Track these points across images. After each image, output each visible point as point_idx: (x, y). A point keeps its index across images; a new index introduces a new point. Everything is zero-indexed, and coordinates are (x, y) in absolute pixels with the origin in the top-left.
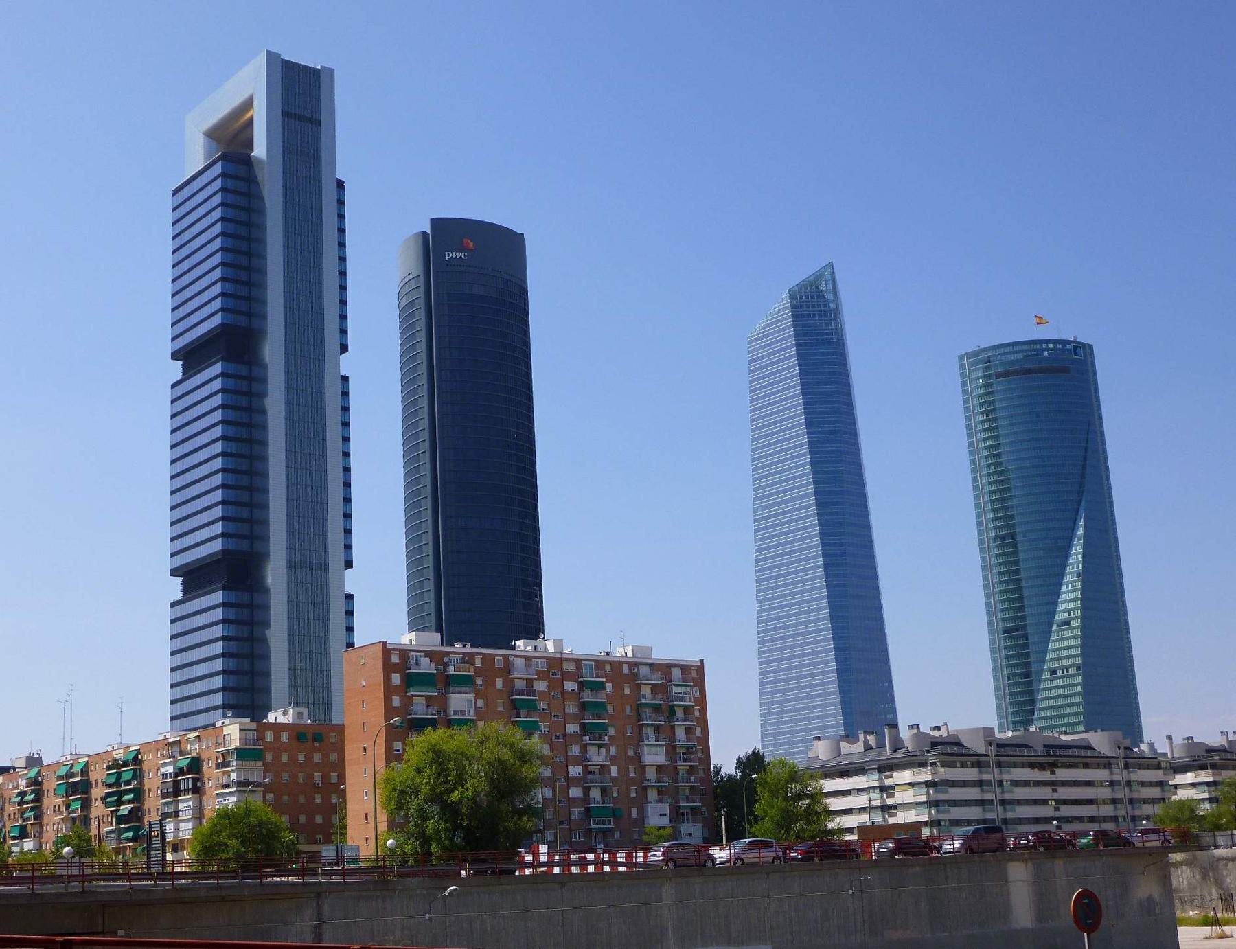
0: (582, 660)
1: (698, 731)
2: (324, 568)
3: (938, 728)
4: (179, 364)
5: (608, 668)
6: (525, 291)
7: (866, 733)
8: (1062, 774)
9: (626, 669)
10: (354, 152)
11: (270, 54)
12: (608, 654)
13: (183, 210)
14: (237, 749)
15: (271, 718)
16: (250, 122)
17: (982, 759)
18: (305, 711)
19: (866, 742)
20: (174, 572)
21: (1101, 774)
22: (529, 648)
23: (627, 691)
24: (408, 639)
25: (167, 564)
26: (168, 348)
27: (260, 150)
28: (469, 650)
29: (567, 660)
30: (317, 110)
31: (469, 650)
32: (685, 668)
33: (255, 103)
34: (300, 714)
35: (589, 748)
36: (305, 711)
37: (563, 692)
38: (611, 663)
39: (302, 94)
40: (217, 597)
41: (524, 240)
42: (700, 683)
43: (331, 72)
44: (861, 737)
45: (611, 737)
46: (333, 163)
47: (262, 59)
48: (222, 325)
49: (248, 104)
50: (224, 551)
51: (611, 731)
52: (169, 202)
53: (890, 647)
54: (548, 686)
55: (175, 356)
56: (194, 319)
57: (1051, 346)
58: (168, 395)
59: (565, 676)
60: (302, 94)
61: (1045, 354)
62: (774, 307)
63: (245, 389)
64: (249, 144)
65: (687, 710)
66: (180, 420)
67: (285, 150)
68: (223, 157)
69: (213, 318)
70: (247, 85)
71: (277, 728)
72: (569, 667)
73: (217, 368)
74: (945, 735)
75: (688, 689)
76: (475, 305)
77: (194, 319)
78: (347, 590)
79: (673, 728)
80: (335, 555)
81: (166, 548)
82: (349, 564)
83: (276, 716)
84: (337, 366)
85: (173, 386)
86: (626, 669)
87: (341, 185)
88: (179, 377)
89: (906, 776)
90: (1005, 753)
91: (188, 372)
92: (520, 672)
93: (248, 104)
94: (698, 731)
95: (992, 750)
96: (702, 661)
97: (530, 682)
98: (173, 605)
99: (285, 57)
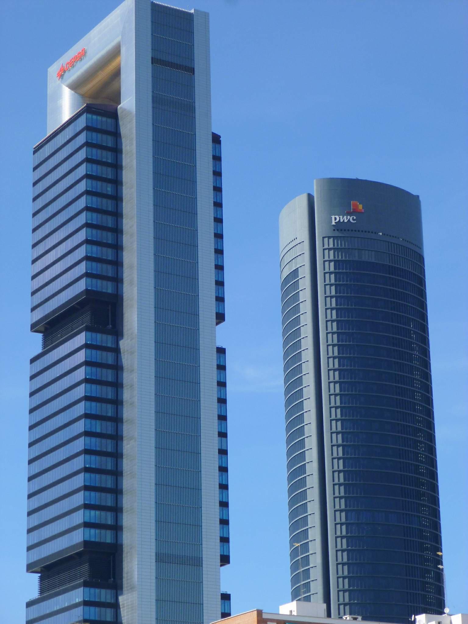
2: (197, 562)
4: (39, 337)
6: (421, 259)
10: (226, 103)
13: (41, 233)
16: (117, 74)
20: (30, 568)
25: (22, 559)
27: (128, 103)
30: (191, 58)
33: (123, 50)
40: (77, 595)
43: (206, 15)
46: (208, 114)
48: (87, 291)
49: (116, 52)
50: (86, 543)
58: (27, 370)
63: (110, 361)
64: (117, 97)
66: (37, 536)
68: (89, 109)
73: (80, 339)
78: (219, 344)
80: (210, 550)
81: (23, 540)
82: (225, 560)
85: (33, 361)
87: (216, 139)
88: (39, 350)
91: (49, 345)
93: (116, 52)
98: (29, 604)
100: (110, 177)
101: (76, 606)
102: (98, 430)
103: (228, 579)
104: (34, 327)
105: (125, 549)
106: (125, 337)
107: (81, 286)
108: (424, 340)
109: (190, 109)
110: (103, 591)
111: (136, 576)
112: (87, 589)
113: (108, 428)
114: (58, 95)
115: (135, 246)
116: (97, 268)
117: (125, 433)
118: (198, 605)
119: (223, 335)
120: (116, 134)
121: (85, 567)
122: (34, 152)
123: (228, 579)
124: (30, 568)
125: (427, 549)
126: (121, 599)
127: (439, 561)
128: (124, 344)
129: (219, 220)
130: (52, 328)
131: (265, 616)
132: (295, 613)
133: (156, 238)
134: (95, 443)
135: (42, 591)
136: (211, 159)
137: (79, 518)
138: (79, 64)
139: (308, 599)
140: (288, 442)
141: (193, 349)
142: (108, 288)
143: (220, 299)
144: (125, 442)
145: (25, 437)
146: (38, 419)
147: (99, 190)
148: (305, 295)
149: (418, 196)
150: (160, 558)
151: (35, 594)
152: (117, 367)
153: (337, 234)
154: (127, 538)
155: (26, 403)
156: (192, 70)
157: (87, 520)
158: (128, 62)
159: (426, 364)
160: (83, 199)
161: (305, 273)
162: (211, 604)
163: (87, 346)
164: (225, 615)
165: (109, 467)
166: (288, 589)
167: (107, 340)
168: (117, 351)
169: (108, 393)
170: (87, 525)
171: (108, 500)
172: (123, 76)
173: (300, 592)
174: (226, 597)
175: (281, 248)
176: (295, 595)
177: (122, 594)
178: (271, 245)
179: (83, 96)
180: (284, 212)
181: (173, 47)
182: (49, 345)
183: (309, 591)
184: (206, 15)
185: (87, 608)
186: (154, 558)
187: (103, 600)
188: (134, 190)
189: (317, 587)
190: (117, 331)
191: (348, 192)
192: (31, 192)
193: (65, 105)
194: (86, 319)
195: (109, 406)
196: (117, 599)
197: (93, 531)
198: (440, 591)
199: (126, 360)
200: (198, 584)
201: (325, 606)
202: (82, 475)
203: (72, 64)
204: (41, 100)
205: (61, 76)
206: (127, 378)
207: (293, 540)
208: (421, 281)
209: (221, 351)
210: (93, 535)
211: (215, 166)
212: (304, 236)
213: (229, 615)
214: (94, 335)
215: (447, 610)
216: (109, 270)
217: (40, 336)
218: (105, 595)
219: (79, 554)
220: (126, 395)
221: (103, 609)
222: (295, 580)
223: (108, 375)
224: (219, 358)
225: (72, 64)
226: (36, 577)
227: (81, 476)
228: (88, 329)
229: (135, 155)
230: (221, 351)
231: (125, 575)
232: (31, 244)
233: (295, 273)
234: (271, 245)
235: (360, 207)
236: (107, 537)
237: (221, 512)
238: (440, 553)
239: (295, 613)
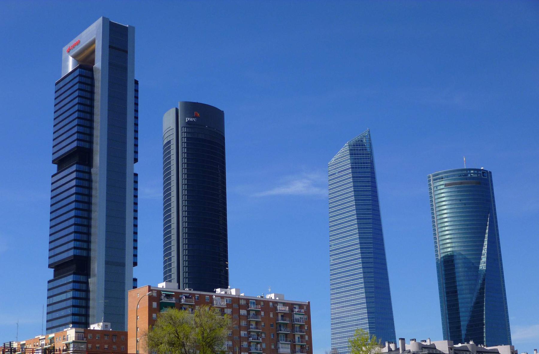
0: (249, 299)
1: (307, 337)
2: (123, 265)
3: (425, 341)
4: (56, 166)
5: (262, 304)
6: (224, 138)
7: (389, 343)
9: (271, 304)
10: (144, 68)
14: (73, 342)
15: (92, 327)
16: (93, 52)
18: (109, 324)
19: (389, 347)
22: (223, 293)
23: (271, 316)
24: (162, 285)
25: (47, 262)
26: (51, 158)
27: (98, 64)
28: (192, 292)
29: (242, 299)
31: (192, 292)
32: (301, 306)
33: (96, 42)
34: (106, 326)
35: (252, 344)
36: (109, 324)
37: (239, 315)
38: (264, 301)
40: (70, 278)
41: (223, 114)
42: (308, 312)
43: (134, 28)
44: (387, 344)
45: (263, 339)
46: (133, 72)
48: (77, 147)
50: (75, 256)
51: (263, 335)
52: (54, 89)
53: (395, 322)
54: (232, 312)
55: (54, 162)
56: (64, 144)
57: (472, 172)
59: (240, 307)
61: (469, 175)
64: (93, 62)
65: (301, 327)
67: (110, 64)
68: (80, 67)
69: (73, 144)
70: (93, 33)
71: (94, 331)
72: (243, 302)
73: (74, 168)
74: (429, 344)
75: (302, 316)
76: (204, 149)
77: (64, 144)
78: (135, 172)
79: (294, 335)
81: (47, 254)
82: (135, 264)
83: (96, 327)
84: (133, 169)
85: (53, 176)
86: (271, 304)
87: (136, 82)
88: (56, 172)
91: (60, 170)
92: (219, 303)
93: (93, 42)
94: (307, 337)
96: (309, 303)
98: (49, 282)
100: (89, 83)
101: (69, 299)
102: (81, 207)
103: (136, 272)
105: (92, 259)
106: (94, 167)
107: (75, 144)
108: (224, 178)
109: (125, 69)
110: (82, 276)
111: (98, 161)
112: (75, 276)
113: (86, 206)
114: (67, 60)
115: (99, 128)
116: (80, 213)
117: (93, 209)
118: (123, 284)
120: (92, 78)
121: (74, 266)
122: (56, 85)
123: (136, 272)
124: (50, 266)
125: (222, 261)
126: (89, 280)
127: (227, 266)
128: (93, 170)
129: (135, 233)
130: (62, 162)
131: (151, 288)
132: (164, 287)
133: (108, 185)
134: (79, 221)
135: (55, 276)
136: (134, 98)
137: (72, 245)
138: (76, 47)
139: (170, 281)
140: (164, 215)
141: (124, 175)
142: (87, 146)
143: (135, 256)
144: (93, 213)
146: (53, 239)
147: (80, 231)
148: (173, 152)
150: (107, 263)
151: (51, 277)
152: (90, 180)
153: (188, 126)
154: (93, 254)
156: (127, 52)
157: (75, 246)
158: (98, 47)
159: (225, 188)
161: (174, 142)
162: (129, 282)
163: (76, 171)
164: (135, 287)
165: (85, 247)
166: (162, 277)
167: (86, 168)
168: (90, 173)
169: (87, 109)
170: (75, 248)
171: (85, 237)
172: (96, 53)
173: (167, 278)
174: (135, 280)
175: (164, 130)
176: (165, 279)
177: (90, 278)
178: (160, 128)
179: (78, 61)
180: (166, 115)
181: (118, 39)
182: (60, 170)
183: (171, 255)
184: (134, 28)
185: (74, 284)
186: (104, 262)
187: (82, 280)
188: (99, 103)
189: (174, 276)
190: (87, 274)
191: (192, 108)
192: (52, 143)
193: (70, 65)
195: (86, 190)
196: (90, 170)
197: (76, 309)
198: (226, 279)
199: (94, 178)
200: (123, 274)
201: (177, 284)
202: (73, 227)
203: (73, 47)
204: (60, 62)
205: (68, 52)
206: (92, 295)
207: (165, 256)
208: (223, 148)
209: (136, 175)
210: (78, 252)
211: (135, 121)
212: (174, 126)
213: (136, 287)
214: (80, 166)
215: (229, 287)
216: (87, 138)
217: (56, 166)
218: (82, 278)
219: (72, 260)
220: (94, 193)
221: (81, 284)
222: (165, 273)
223: (86, 184)
224: (135, 178)
225: (73, 47)
226: (52, 270)
227: (72, 250)
228: (77, 163)
229: (100, 74)
230: (136, 175)
231: (91, 270)
232: (54, 97)
233: (169, 142)
234: (160, 128)
235: (198, 114)
236: (84, 253)
237: (134, 207)
239: (164, 287)
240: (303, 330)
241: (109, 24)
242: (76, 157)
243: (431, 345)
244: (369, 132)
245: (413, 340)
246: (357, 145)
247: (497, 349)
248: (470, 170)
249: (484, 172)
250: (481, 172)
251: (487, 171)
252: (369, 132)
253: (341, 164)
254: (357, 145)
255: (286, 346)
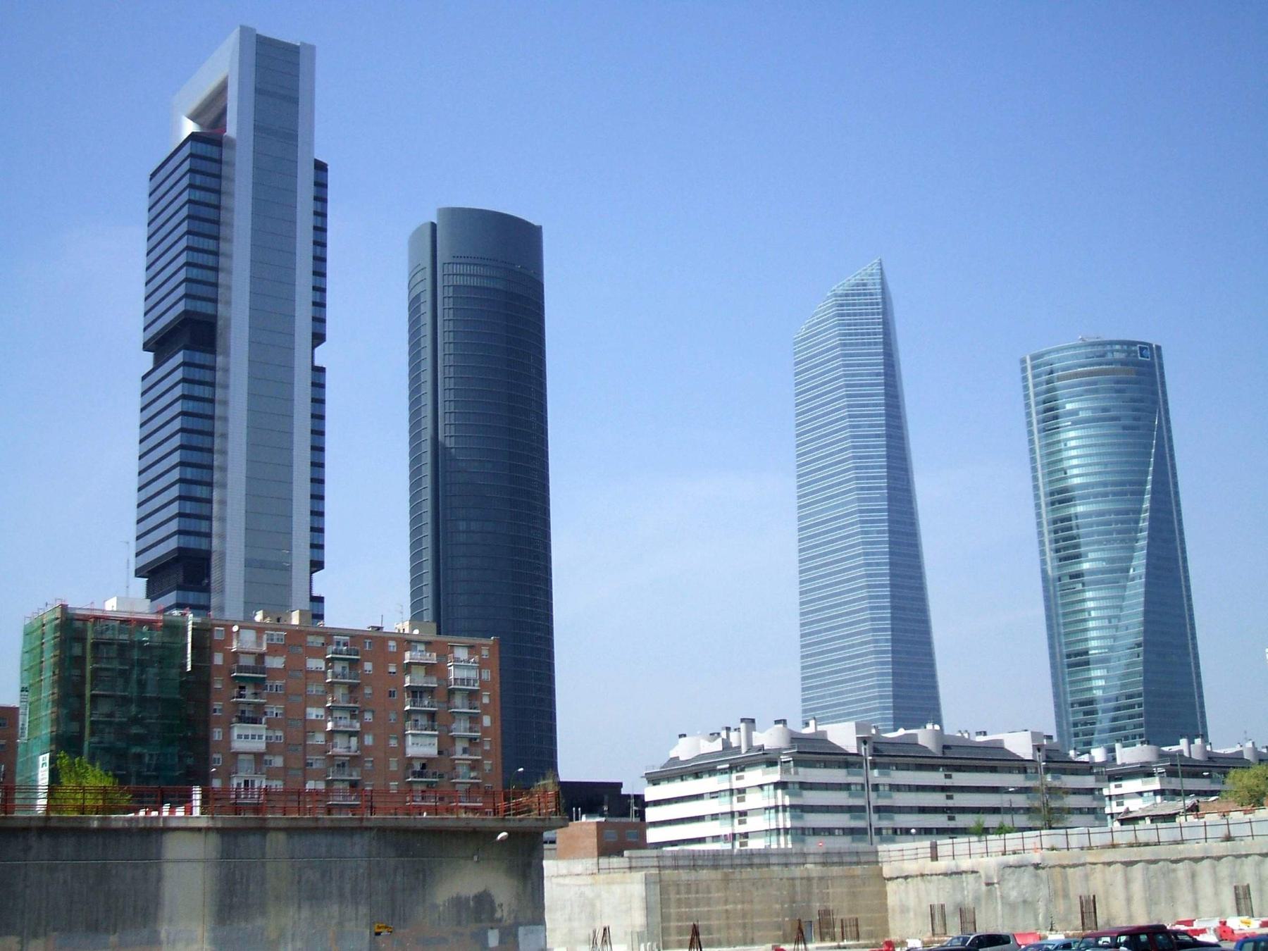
4: (150, 356)
8: (960, 779)
10: (329, 133)
11: (244, 31)
12: (379, 629)
16: (223, 113)
17: (850, 759)
21: (1016, 780)
26: (139, 338)
39: (278, 71)
43: (313, 48)
47: (234, 38)
58: (138, 387)
60: (278, 71)
62: (810, 309)
70: (222, 65)
76: (491, 309)
85: (144, 378)
87: (321, 167)
88: (151, 367)
89: (754, 776)
90: (883, 754)
91: (158, 363)
95: (1040, 757)
97: (260, 657)
99: (260, 32)
104: (139, 573)
119: (322, 356)
124: (139, 573)
141: (289, 367)
145: (133, 515)
149: (540, 228)
155: (134, 465)
160: (178, 437)
184: (313, 48)
194: (179, 577)
238: (476, 858)
240: (477, 704)
241: (254, 40)
242: (186, 337)
243: (817, 732)
244: (881, 264)
245: (777, 722)
246: (853, 295)
247: (1001, 741)
248: (1112, 343)
249: (1145, 347)
250: (1137, 348)
251: (1150, 345)
252: (881, 264)
253: (821, 338)
254: (853, 295)
255: (428, 740)
